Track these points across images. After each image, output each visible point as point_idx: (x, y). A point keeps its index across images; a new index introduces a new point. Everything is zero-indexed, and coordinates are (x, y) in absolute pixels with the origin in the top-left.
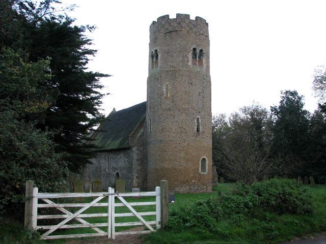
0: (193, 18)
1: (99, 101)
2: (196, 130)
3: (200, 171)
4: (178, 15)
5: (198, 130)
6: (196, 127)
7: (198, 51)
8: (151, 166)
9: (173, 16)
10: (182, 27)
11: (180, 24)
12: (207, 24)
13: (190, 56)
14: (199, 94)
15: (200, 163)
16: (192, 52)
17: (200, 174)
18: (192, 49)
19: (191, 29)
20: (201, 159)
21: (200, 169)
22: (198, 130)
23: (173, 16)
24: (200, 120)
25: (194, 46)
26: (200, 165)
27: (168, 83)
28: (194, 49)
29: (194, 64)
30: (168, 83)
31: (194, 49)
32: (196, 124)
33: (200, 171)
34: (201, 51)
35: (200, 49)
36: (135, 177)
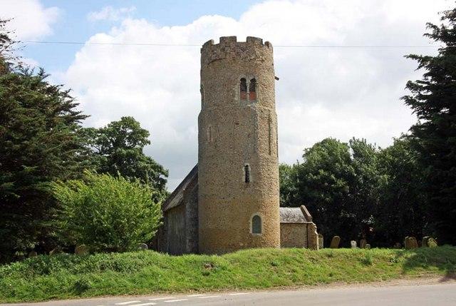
0: (217, 42)
1: (74, 114)
2: (244, 180)
3: (251, 232)
4: (222, 39)
5: (247, 180)
6: (244, 177)
7: (248, 82)
8: (201, 226)
9: (241, 39)
10: (226, 54)
11: (223, 50)
12: (202, 50)
13: (237, 89)
14: (249, 136)
15: (251, 221)
16: (239, 84)
17: (251, 236)
18: (239, 80)
19: (238, 54)
20: (252, 217)
21: (251, 229)
22: (247, 180)
23: (241, 39)
24: (249, 168)
25: (243, 76)
26: (251, 225)
27: (210, 125)
28: (243, 80)
29: (243, 98)
30: (210, 125)
31: (243, 80)
32: (244, 173)
33: (251, 232)
34: (253, 81)
35: (251, 78)
36: (187, 241)
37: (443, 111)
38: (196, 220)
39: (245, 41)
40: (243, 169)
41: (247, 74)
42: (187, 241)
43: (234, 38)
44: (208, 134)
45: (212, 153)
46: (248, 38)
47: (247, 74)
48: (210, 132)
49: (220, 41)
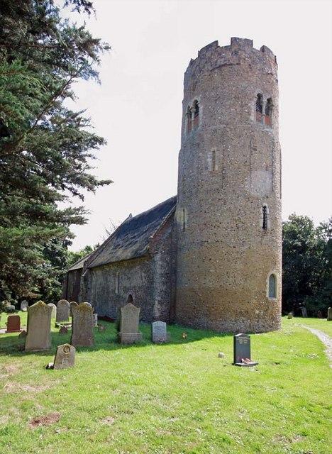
3: (267, 296)
5: (264, 227)
7: (265, 100)
9: (224, 42)
11: (236, 53)
15: (268, 281)
22: (264, 227)
23: (224, 42)
26: (268, 286)
28: (260, 96)
29: (259, 120)
31: (260, 96)
33: (267, 296)
34: (269, 100)
35: (268, 97)
36: (156, 302)
37: (10, 306)
38: (172, 275)
39: (229, 43)
40: (261, 209)
41: (264, 90)
42: (156, 302)
43: (249, 43)
44: (209, 160)
45: (216, 186)
46: (234, 40)
47: (264, 90)
48: (214, 158)
49: (232, 42)
